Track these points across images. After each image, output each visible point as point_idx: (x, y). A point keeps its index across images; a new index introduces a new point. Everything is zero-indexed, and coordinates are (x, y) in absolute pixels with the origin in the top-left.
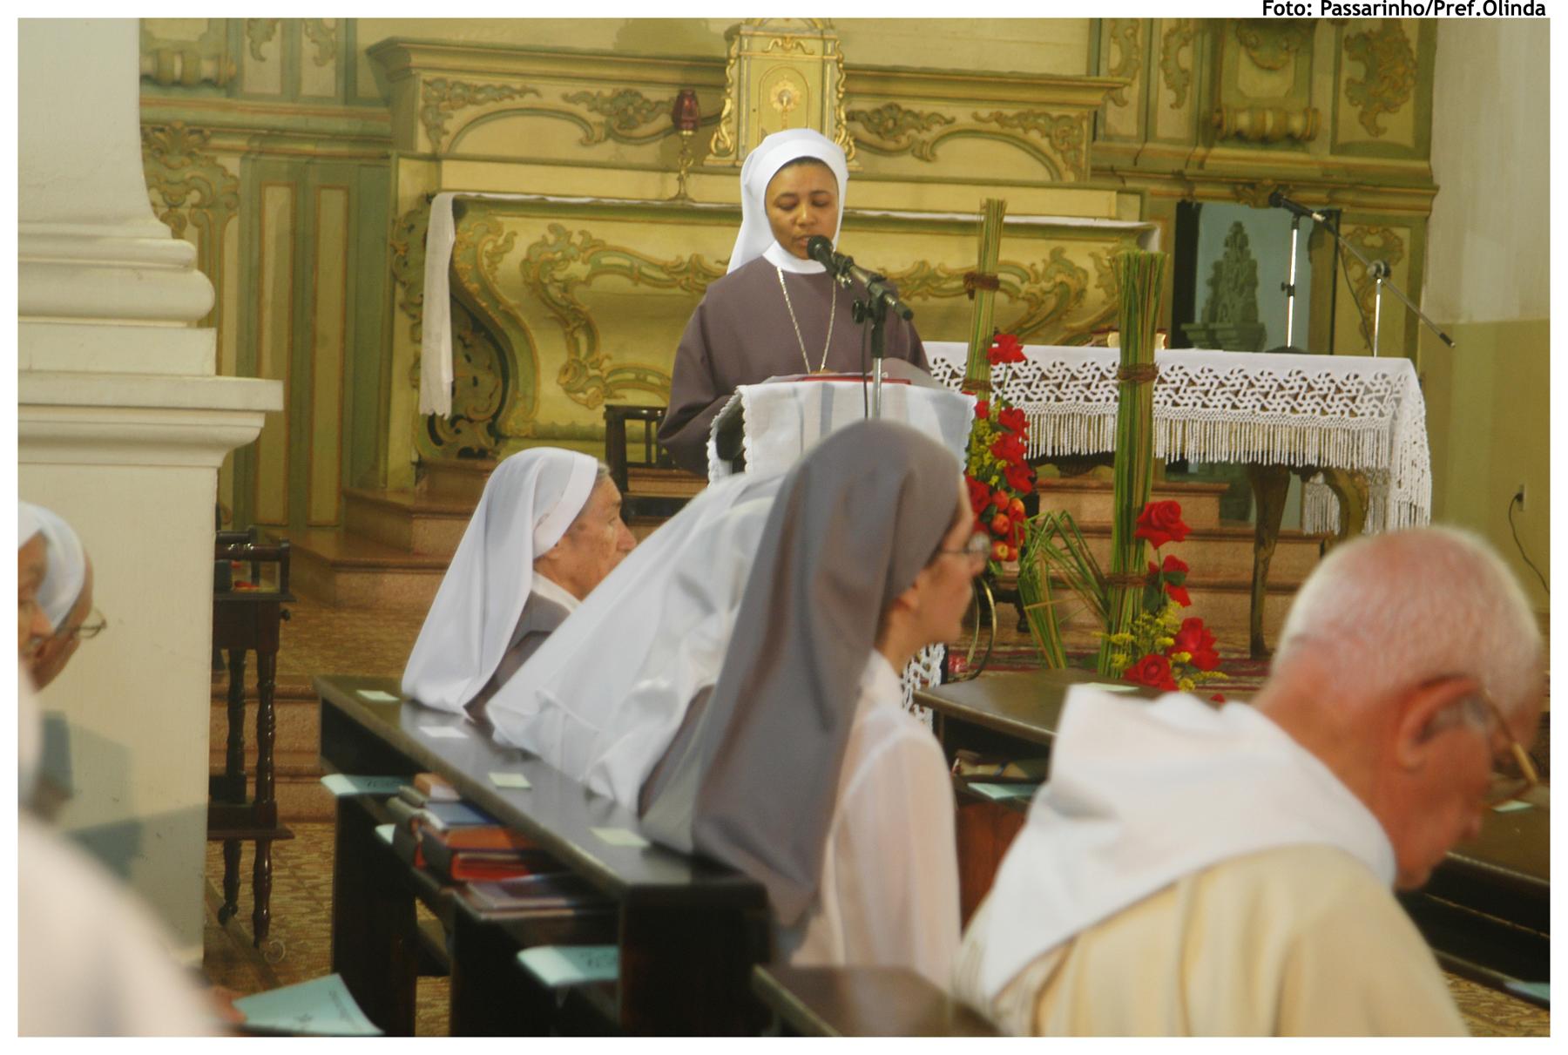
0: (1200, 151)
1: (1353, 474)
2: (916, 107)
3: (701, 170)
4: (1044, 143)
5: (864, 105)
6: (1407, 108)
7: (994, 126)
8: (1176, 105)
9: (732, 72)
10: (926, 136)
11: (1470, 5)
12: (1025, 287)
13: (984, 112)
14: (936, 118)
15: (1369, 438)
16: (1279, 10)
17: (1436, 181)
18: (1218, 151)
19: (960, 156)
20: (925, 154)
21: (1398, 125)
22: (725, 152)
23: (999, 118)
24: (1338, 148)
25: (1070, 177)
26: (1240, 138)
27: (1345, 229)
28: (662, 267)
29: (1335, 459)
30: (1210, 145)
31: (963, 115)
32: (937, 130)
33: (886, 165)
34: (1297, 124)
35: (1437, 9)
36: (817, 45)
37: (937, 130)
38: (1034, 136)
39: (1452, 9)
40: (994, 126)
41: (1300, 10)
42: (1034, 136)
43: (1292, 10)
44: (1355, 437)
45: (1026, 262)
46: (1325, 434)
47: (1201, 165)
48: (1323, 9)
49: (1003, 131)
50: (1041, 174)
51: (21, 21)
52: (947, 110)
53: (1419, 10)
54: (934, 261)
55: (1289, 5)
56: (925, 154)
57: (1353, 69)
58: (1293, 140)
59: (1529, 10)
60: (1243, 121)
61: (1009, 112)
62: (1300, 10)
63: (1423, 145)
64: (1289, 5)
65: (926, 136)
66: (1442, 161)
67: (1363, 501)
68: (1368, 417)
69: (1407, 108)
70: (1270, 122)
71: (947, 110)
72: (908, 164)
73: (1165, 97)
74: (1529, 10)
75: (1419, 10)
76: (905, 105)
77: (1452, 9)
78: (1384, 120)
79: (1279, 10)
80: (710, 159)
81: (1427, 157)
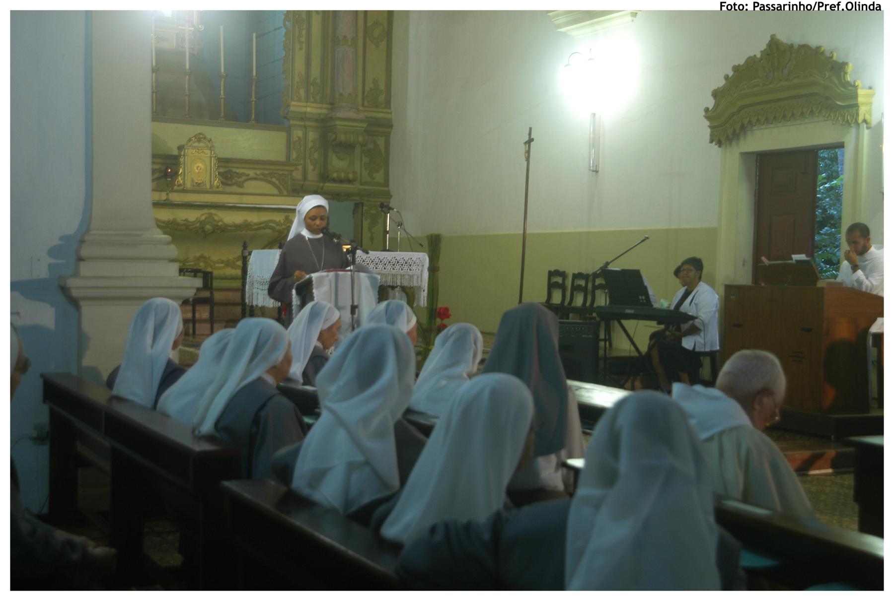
0: (321, 184)
1: (411, 288)
2: (238, 171)
3: (173, 191)
4: (277, 182)
5: (222, 170)
6: (382, 171)
7: (262, 177)
8: (314, 170)
9: (182, 160)
10: (240, 180)
11: (838, 5)
12: (278, 228)
13: (258, 172)
14: (244, 174)
15: (415, 277)
16: (729, 7)
17: (392, 193)
18: (327, 184)
19: (250, 186)
20: (240, 185)
21: (379, 177)
22: (180, 185)
23: (263, 174)
24: (361, 184)
25: (285, 193)
26: (334, 180)
27: (365, 208)
28: (164, 222)
29: (406, 284)
30: (324, 183)
31: (252, 173)
32: (244, 178)
33: (228, 189)
34: (351, 176)
35: (819, 7)
36: (208, 152)
37: (244, 178)
38: (274, 180)
39: (828, 7)
40: (262, 177)
41: (741, 7)
42: (274, 180)
43: (737, 7)
44: (411, 277)
45: (277, 219)
46: (402, 276)
47: (322, 188)
48: (754, 7)
49: (265, 178)
50: (276, 192)
51: (12, 12)
52: (247, 172)
53: (809, 7)
54: (249, 220)
55: (735, 4)
56: (240, 185)
57: (366, 160)
58: (349, 181)
59: (872, 7)
60: (335, 175)
61: (266, 172)
62: (741, 7)
63: (386, 183)
64: (735, 4)
65: (240, 180)
66: (393, 187)
67: (414, 296)
68: (415, 270)
69: (382, 171)
70: (343, 176)
71: (247, 172)
72: (235, 189)
73: (310, 167)
74: (872, 7)
75: (809, 7)
76: (234, 170)
77: (828, 7)
78: (375, 175)
79: (729, 7)
80: (175, 188)
81: (388, 186)
